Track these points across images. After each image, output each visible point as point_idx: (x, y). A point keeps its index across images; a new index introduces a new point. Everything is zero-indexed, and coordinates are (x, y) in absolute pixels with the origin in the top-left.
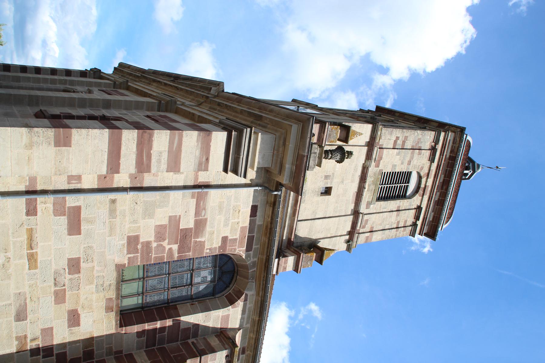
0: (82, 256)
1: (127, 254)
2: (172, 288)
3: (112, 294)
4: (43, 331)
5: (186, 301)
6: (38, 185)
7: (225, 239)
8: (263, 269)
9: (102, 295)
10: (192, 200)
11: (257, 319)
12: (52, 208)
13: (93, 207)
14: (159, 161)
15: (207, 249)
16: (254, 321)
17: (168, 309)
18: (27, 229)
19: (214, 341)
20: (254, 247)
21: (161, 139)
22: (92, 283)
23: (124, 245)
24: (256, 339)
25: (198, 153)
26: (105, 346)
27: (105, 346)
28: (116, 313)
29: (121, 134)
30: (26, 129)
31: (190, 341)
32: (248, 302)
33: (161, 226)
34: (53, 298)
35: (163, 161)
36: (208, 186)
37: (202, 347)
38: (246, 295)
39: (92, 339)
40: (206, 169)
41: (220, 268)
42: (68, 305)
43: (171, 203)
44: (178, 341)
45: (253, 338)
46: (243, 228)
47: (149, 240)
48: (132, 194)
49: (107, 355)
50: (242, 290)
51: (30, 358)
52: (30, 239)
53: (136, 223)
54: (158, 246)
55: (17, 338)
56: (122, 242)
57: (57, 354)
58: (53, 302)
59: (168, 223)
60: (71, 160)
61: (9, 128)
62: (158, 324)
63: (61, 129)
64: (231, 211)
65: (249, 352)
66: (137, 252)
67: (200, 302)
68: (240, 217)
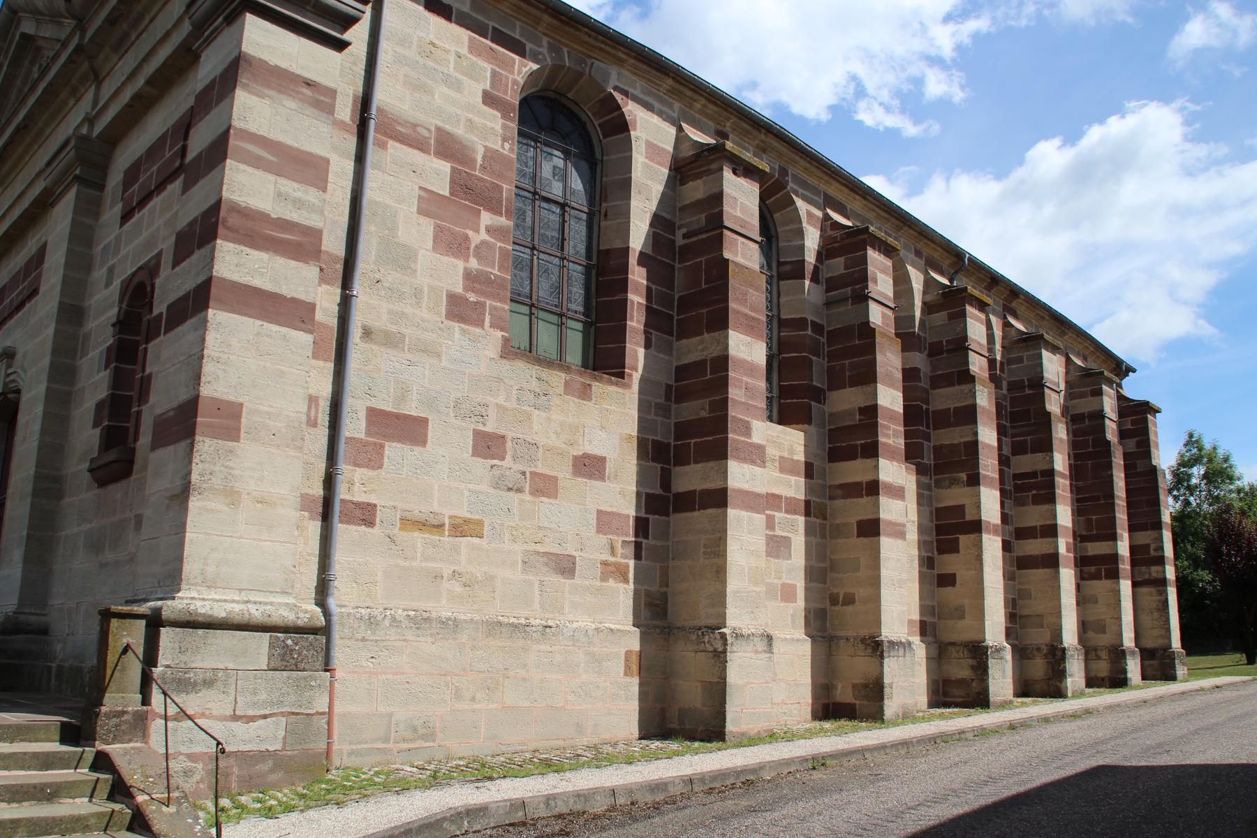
0: (472, 426)
1: (483, 327)
2: (562, 250)
3: (558, 379)
4: (600, 529)
5: (596, 228)
6: (310, 492)
7: (489, 99)
8: (572, 30)
9: (556, 400)
10: (390, 150)
11: (670, 82)
12: (365, 471)
13: (375, 379)
14: (299, 204)
15: (503, 148)
16: (671, 91)
17: (605, 272)
18: (400, 529)
19: (696, 190)
20: (518, 37)
21: (244, 185)
22: (529, 417)
23: (464, 332)
24: (709, 100)
25: (290, 104)
26: (652, 417)
27: (652, 417)
28: (595, 379)
29: (224, 280)
30: (192, 498)
31: (680, 241)
32: (631, 90)
33: (436, 237)
34: (545, 500)
35: (298, 194)
36: (365, 102)
37: (700, 219)
38: (616, 88)
39: (642, 444)
40: (332, 93)
41: (541, 128)
42: (563, 473)
43: (389, 202)
44: (673, 267)
45: (704, 106)
46: (473, 48)
47: (461, 271)
48: (358, 288)
49: (668, 417)
50: (602, 95)
51: (643, 562)
52: (422, 525)
53: (421, 292)
54: (478, 256)
55: (604, 578)
56: (457, 335)
57: (647, 512)
58: (551, 501)
59: (432, 221)
60: (272, 410)
61: (187, 534)
62: (636, 299)
63: (199, 419)
64: (430, 64)
65: (728, 124)
66: (483, 305)
67: (604, 197)
68: (447, 46)
